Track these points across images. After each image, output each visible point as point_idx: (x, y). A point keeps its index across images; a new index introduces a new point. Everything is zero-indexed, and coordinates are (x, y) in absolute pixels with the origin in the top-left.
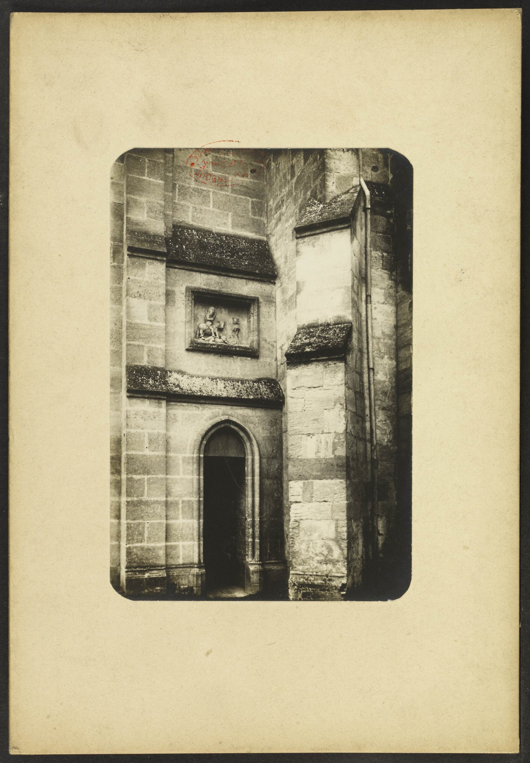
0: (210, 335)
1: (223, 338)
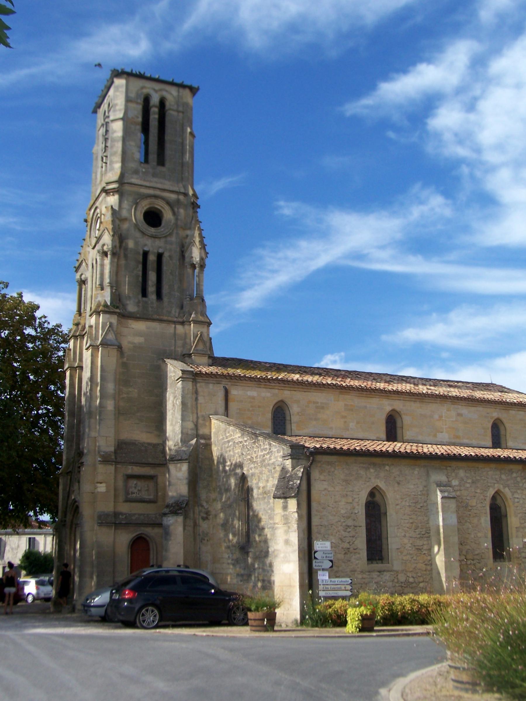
0: (134, 493)
1: (140, 494)
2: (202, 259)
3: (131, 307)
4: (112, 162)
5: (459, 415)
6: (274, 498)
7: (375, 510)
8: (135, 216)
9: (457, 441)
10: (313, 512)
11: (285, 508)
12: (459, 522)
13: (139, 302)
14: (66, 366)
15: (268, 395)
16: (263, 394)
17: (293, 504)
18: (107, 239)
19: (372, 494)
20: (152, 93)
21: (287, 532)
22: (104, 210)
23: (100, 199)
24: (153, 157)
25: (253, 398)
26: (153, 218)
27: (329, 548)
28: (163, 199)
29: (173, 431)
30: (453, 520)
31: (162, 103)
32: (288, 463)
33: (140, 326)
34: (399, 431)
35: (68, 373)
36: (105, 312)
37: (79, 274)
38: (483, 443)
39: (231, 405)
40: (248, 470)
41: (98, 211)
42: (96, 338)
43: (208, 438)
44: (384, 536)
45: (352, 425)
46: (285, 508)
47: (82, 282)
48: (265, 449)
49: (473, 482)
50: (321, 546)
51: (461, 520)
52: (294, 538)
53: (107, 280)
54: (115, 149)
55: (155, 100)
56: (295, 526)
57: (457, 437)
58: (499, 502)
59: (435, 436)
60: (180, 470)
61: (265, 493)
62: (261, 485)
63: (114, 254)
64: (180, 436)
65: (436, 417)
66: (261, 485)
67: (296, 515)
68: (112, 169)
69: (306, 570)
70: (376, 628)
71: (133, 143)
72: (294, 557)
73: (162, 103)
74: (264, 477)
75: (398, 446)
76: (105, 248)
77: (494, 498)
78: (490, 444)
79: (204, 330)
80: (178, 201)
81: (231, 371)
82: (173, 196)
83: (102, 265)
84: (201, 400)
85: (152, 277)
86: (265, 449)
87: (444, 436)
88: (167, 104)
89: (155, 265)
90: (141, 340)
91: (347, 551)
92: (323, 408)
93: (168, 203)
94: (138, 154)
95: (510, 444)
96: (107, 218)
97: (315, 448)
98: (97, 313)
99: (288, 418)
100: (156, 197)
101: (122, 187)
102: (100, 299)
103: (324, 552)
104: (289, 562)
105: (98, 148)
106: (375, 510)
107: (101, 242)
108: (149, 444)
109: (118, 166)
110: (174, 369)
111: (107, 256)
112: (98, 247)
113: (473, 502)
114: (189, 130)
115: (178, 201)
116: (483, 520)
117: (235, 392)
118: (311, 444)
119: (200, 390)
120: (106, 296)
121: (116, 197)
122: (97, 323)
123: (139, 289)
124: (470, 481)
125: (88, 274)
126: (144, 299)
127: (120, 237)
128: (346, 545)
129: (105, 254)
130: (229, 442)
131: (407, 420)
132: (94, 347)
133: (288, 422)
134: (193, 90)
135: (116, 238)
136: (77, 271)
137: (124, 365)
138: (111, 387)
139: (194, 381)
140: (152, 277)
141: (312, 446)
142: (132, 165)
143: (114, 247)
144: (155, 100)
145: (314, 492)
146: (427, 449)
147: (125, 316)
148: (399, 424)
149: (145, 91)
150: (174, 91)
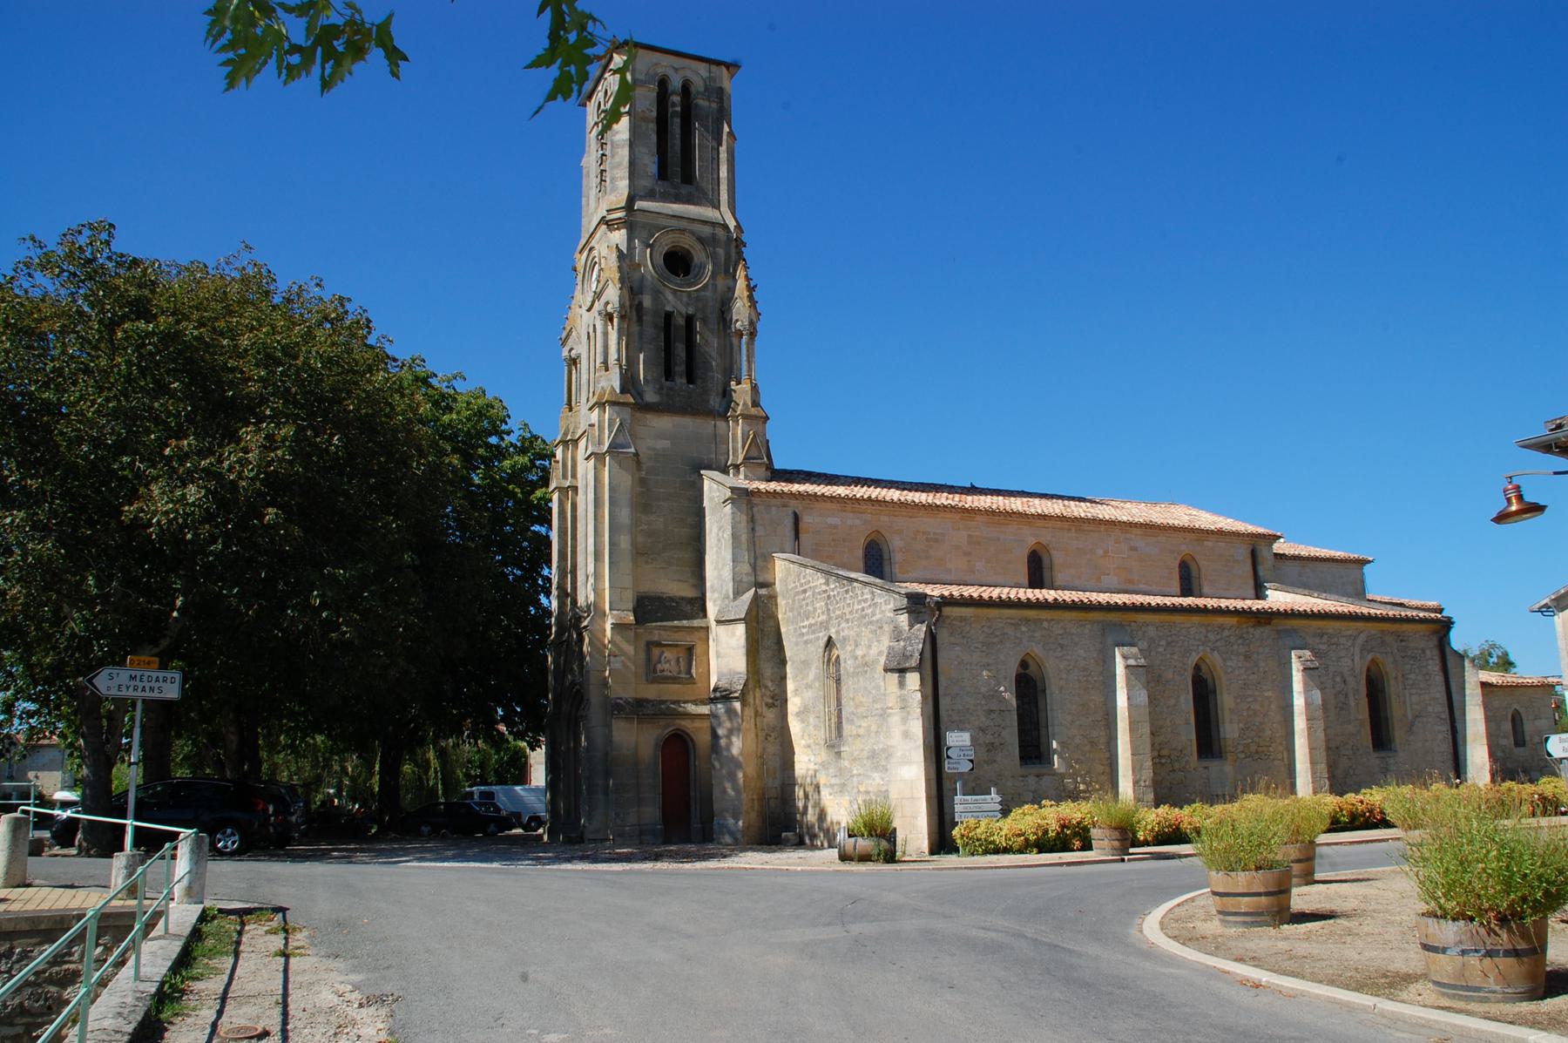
2: (751, 323)
3: (651, 397)
4: (613, 180)
5: (1134, 549)
6: (886, 670)
7: (1029, 687)
8: (648, 264)
9: (1131, 587)
10: (941, 692)
11: (902, 684)
12: (1150, 701)
13: (662, 388)
14: (553, 486)
15: (857, 522)
16: (850, 522)
17: (913, 679)
18: (613, 294)
19: (1024, 664)
20: (670, 72)
21: (904, 721)
22: (605, 251)
23: (598, 235)
24: (675, 169)
25: (836, 527)
26: (678, 263)
27: (968, 743)
28: (693, 233)
29: (719, 577)
30: (1142, 697)
31: (686, 88)
32: (904, 619)
33: (664, 423)
34: (1046, 574)
35: (555, 497)
36: (613, 403)
37: (567, 348)
38: (1168, 590)
39: (803, 536)
40: (837, 632)
41: (595, 253)
42: (600, 443)
43: (769, 585)
44: (1042, 723)
45: (979, 566)
46: (902, 684)
47: (574, 362)
48: (865, 601)
49: (1168, 644)
50: (957, 740)
51: (1152, 700)
52: (917, 727)
53: (613, 356)
54: (617, 159)
55: (676, 83)
56: (919, 711)
57: (1131, 582)
58: (1204, 673)
59: (1099, 579)
60: (734, 634)
61: (866, 664)
62: (859, 652)
63: (622, 317)
64: (731, 585)
65: (1100, 552)
66: (859, 652)
67: (919, 695)
68: (614, 189)
69: (933, 776)
70: (1131, 850)
71: (645, 150)
72: (918, 755)
73: (686, 88)
74: (864, 641)
75: (1050, 595)
76: (609, 308)
77: (1197, 668)
78: (1178, 590)
79: (760, 427)
80: (714, 237)
81: (796, 487)
82: (707, 230)
83: (606, 334)
84: (760, 531)
85: (680, 350)
86: (865, 601)
87: (1112, 580)
88: (693, 89)
89: (683, 333)
90: (667, 444)
91: (991, 747)
92: (936, 541)
93: (700, 240)
94: (650, 165)
95: (1206, 590)
96: (612, 261)
97: (942, 596)
98: (601, 405)
99: (886, 556)
100: (682, 231)
101: (631, 219)
102: (603, 383)
103: (961, 748)
104: (909, 763)
105: (590, 161)
106: (1029, 687)
107: (603, 299)
108: (683, 598)
109: (623, 185)
110: (714, 488)
111: (611, 320)
112: (598, 306)
113: (1169, 675)
114: (726, 129)
115: (714, 237)
116: (1182, 699)
117: (807, 520)
118: (934, 591)
119: (757, 517)
120: (613, 380)
121: (624, 231)
122: (601, 422)
123: (661, 370)
124: (1163, 643)
125: (581, 349)
126: (668, 384)
127: (632, 286)
128: (989, 739)
129: (610, 317)
130: (805, 591)
131: (1058, 557)
132: (598, 457)
133: (886, 563)
134: (732, 67)
135: (626, 292)
136: (563, 344)
137: (643, 482)
138: (625, 514)
139: (750, 505)
140: (680, 350)
141: (936, 593)
142: (646, 183)
143: (622, 305)
144: (676, 83)
145: (941, 661)
146: (1095, 597)
147: (642, 407)
148: (1046, 562)
149: (660, 70)
150: (702, 69)
